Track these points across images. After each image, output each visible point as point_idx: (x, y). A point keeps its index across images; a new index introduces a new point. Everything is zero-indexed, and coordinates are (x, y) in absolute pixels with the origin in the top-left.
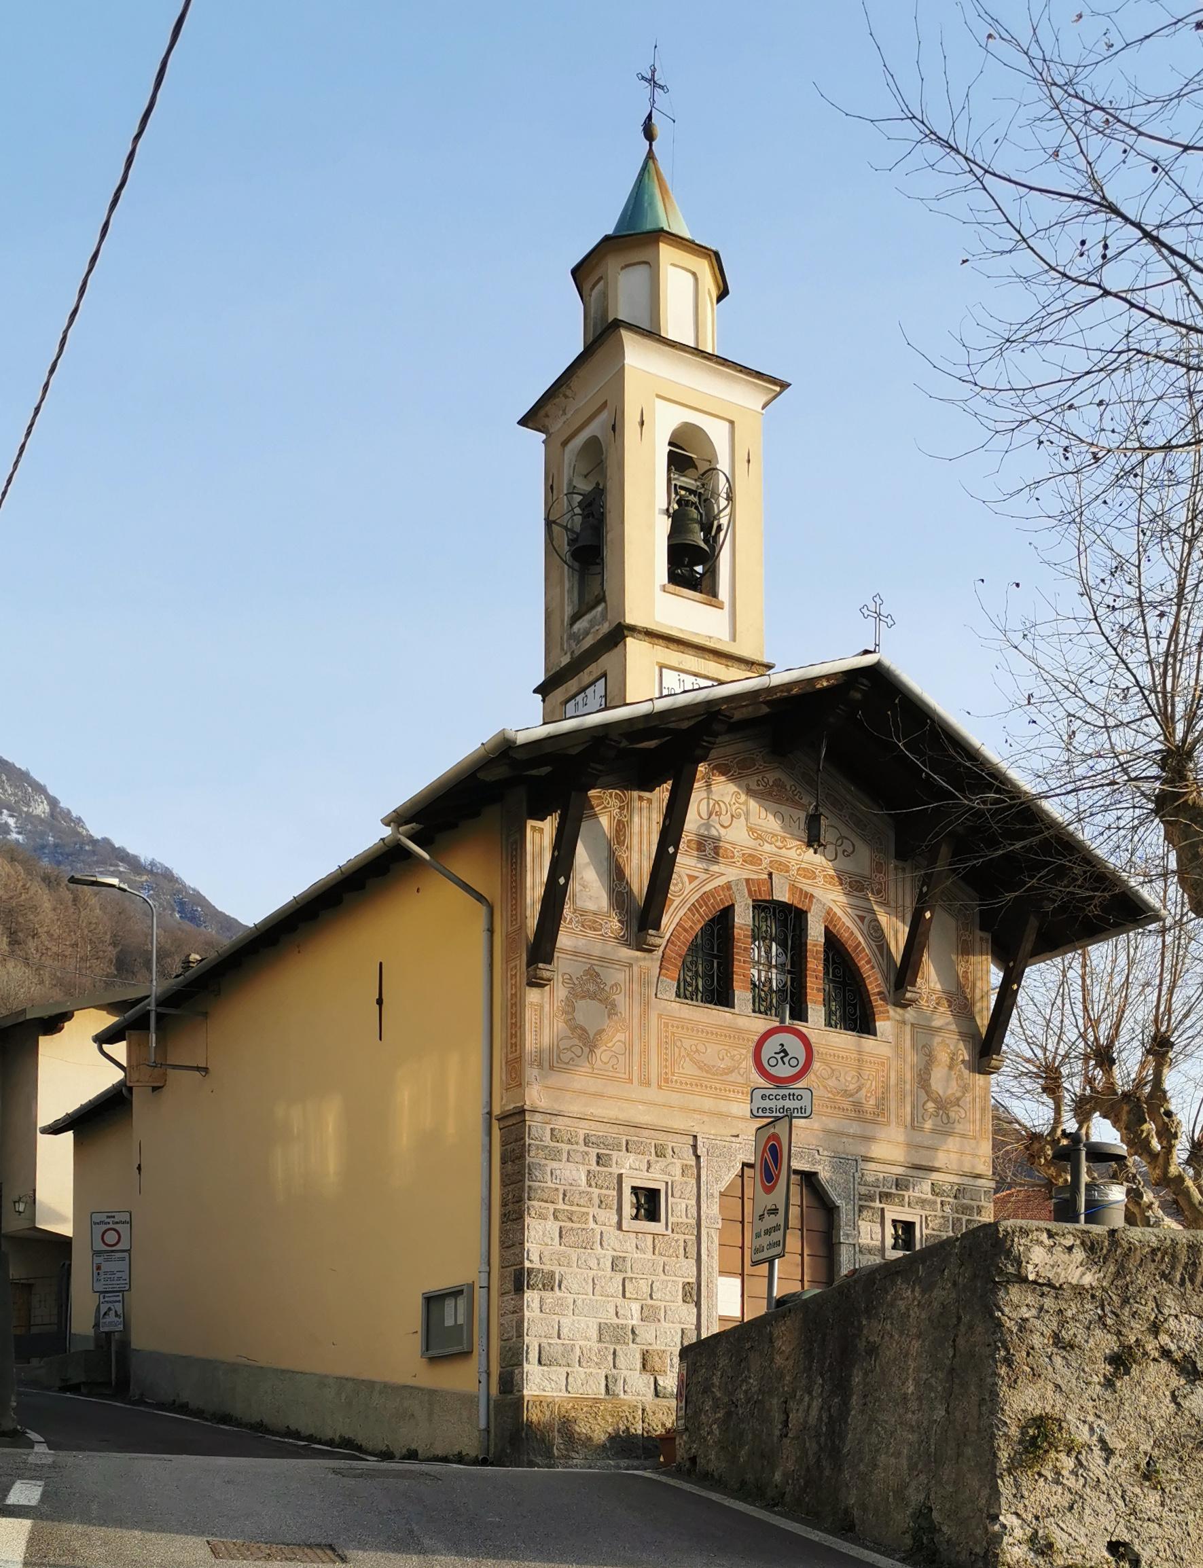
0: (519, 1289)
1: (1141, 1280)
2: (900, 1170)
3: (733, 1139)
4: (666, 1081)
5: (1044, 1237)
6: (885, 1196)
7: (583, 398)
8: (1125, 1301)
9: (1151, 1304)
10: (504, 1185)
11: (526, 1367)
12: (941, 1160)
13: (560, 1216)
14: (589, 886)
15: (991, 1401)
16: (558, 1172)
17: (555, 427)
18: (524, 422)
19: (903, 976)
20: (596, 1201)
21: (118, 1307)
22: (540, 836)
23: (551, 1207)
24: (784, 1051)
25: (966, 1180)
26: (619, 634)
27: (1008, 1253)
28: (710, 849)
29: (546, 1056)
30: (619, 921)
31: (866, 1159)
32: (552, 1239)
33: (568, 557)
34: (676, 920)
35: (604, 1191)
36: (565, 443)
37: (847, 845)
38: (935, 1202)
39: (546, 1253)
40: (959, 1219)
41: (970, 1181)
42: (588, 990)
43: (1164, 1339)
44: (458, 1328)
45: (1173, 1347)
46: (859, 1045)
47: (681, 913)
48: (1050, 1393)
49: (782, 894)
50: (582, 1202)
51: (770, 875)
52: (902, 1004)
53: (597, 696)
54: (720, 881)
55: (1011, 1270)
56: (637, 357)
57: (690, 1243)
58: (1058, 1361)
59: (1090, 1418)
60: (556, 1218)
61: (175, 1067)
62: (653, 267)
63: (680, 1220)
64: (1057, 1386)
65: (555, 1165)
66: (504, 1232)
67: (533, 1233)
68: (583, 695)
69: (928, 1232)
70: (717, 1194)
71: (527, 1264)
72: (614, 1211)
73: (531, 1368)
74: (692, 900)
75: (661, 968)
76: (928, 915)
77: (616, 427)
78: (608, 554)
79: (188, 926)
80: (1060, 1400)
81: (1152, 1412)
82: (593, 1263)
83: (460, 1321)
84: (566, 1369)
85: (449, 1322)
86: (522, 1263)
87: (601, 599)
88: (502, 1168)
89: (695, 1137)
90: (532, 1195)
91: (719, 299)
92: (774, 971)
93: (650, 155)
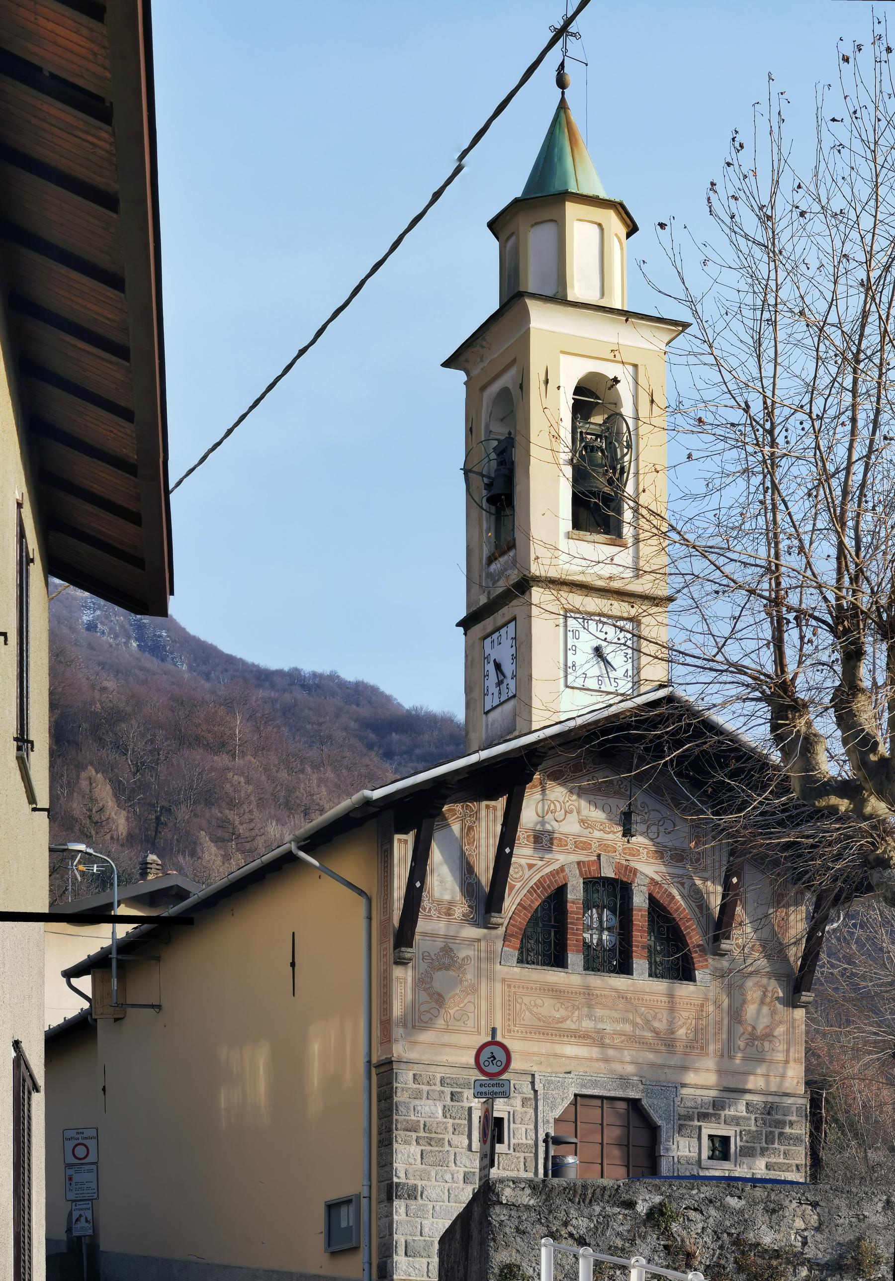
0: (390, 1199)
1: (558, 1202)
2: (713, 1093)
3: (566, 1075)
4: (509, 1031)
5: (511, 1184)
6: (703, 1116)
7: (496, 351)
8: (550, 1212)
9: (563, 1213)
10: (380, 1118)
11: (395, 1258)
12: (753, 1083)
13: (421, 1142)
14: (442, 883)
15: (485, 1258)
16: (419, 1108)
17: (475, 372)
18: (447, 364)
19: (720, 927)
20: (451, 1130)
21: (88, 1214)
22: (403, 847)
23: (414, 1135)
24: (493, 1057)
25: (770, 1099)
26: (524, 585)
27: (494, 1191)
28: (544, 840)
29: (409, 1018)
30: (469, 906)
31: (684, 1085)
32: (415, 1160)
33: (485, 505)
34: (518, 901)
35: (457, 1121)
36: (483, 388)
37: (669, 825)
38: (750, 1119)
39: (410, 1171)
40: (772, 1133)
41: (777, 1099)
42: (444, 963)
43: (570, 1228)
44: (349, 1228)
45: (575, 1232)
46: (671, 996)
47: (521, 895)
48: (514, 1254)
49: (608, 872)
50: (439, 1130)
51: (599, 856)
52: (719, 953)
53: (509, 638)
54: (556, 866)
55: (494, 1199)
56: (542, 320)
57: (529, 1160)
58: (518, 1239)
59: (534, 1265)
60: (418, 1143)
61: (133, 1006)
62: (560, 224)
63: (521, 1141)
64: (518, 1251)
65: (417, 1102)
66: (380, 1155)
67: (399, 1156)
68: (497, 634)
69: (742, 1144)
70: (552, 1121)
71: (395, 1180)
72: (466, 1137)
73: (400, 1260)
74: (531, 883)
75: (504, 941)
76: (735, 880)
77: (523, 386)
78: (516, 503)
79: (151, 662)
80: (519, 1256)
81: (564, 1262)
82: (448, 1177)
83: (351, 1224)
84: (427, 1260)
85: (344, 1224)
86: (392, 1179)
87: (512, 546)
88: (378, 1105)
89: (533, 1075)
90: (399, 1126)
91: (629, 235)
92: (606, 933)
93: (563, 106)
